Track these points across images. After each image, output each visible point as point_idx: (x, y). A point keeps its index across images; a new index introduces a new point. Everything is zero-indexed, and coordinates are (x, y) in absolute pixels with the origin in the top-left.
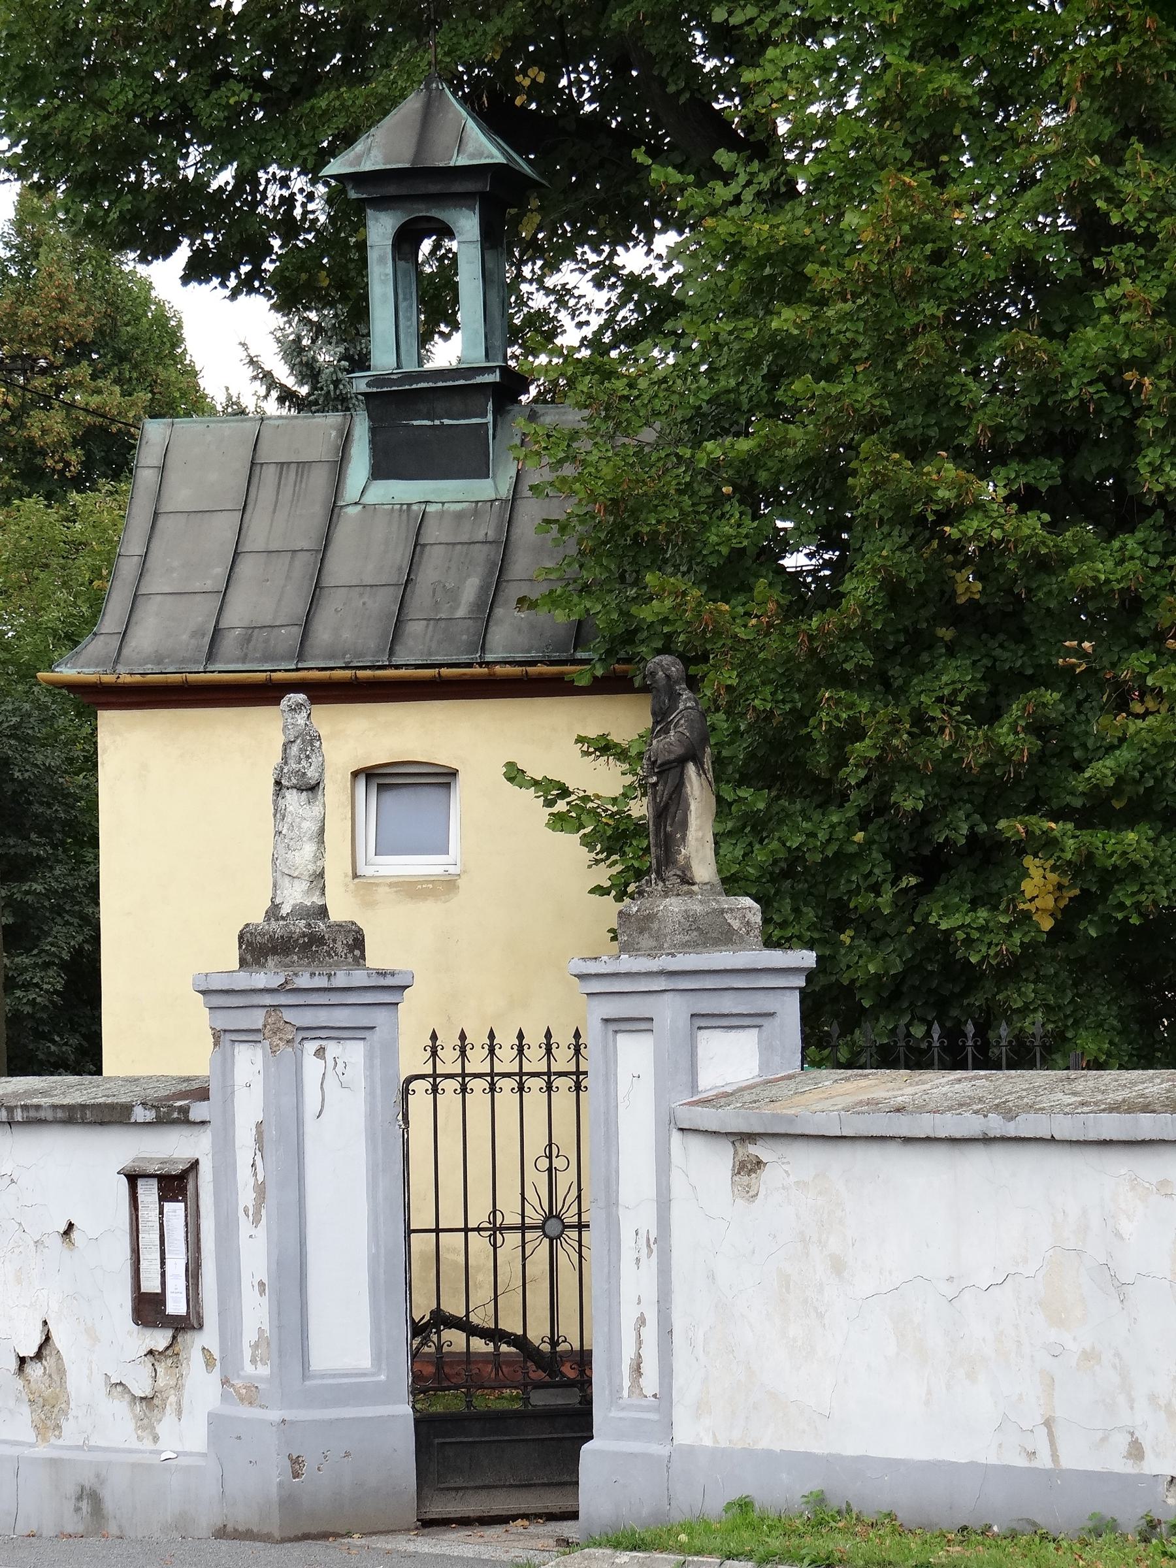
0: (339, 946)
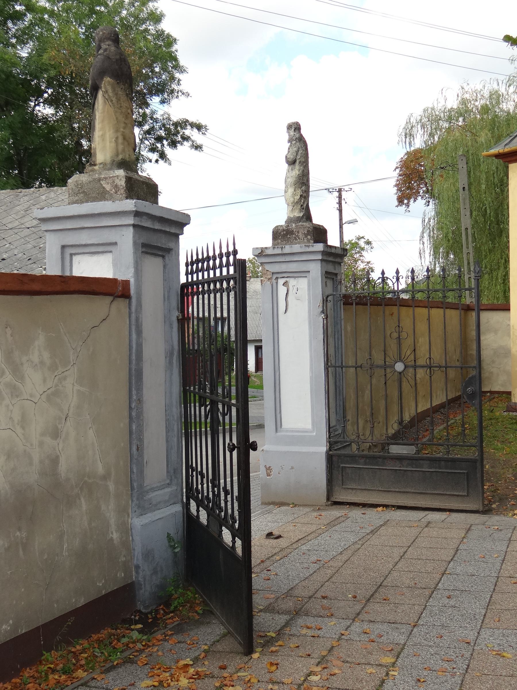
0: (300, 235)
